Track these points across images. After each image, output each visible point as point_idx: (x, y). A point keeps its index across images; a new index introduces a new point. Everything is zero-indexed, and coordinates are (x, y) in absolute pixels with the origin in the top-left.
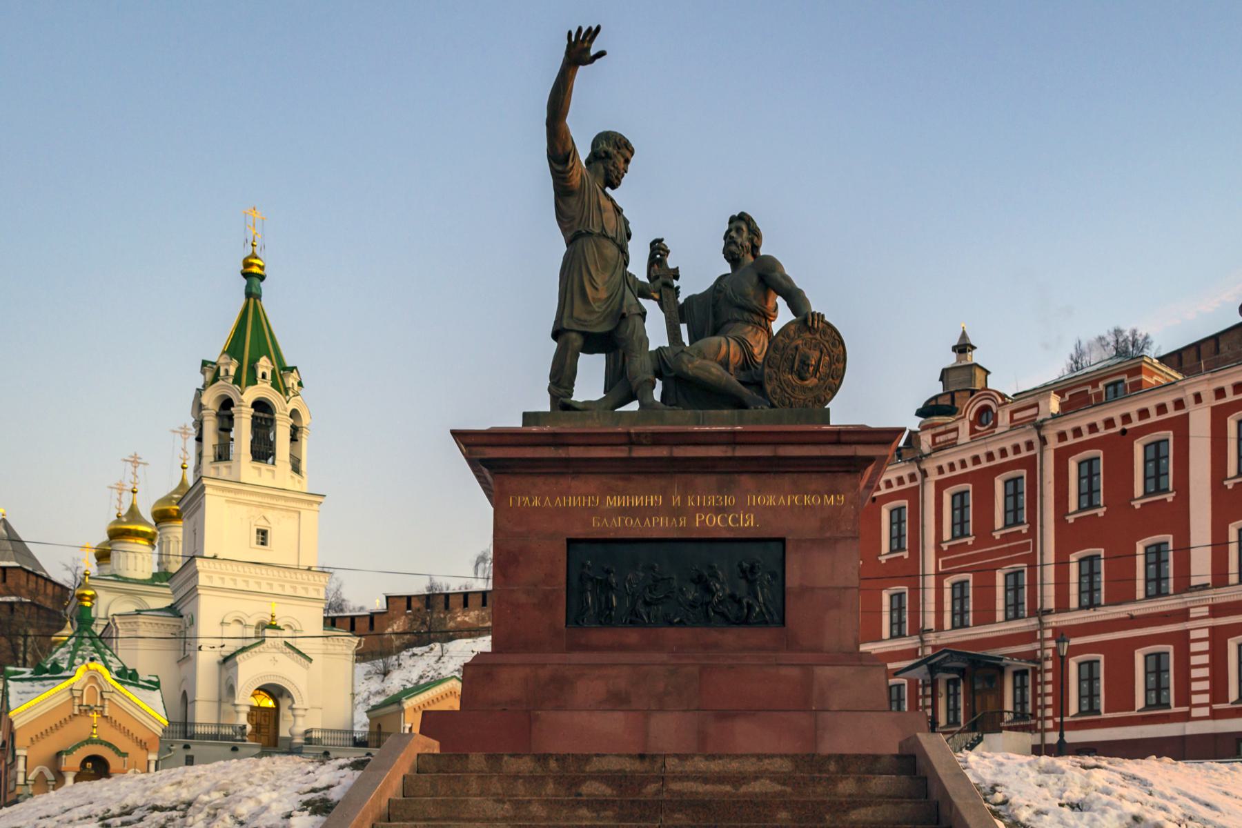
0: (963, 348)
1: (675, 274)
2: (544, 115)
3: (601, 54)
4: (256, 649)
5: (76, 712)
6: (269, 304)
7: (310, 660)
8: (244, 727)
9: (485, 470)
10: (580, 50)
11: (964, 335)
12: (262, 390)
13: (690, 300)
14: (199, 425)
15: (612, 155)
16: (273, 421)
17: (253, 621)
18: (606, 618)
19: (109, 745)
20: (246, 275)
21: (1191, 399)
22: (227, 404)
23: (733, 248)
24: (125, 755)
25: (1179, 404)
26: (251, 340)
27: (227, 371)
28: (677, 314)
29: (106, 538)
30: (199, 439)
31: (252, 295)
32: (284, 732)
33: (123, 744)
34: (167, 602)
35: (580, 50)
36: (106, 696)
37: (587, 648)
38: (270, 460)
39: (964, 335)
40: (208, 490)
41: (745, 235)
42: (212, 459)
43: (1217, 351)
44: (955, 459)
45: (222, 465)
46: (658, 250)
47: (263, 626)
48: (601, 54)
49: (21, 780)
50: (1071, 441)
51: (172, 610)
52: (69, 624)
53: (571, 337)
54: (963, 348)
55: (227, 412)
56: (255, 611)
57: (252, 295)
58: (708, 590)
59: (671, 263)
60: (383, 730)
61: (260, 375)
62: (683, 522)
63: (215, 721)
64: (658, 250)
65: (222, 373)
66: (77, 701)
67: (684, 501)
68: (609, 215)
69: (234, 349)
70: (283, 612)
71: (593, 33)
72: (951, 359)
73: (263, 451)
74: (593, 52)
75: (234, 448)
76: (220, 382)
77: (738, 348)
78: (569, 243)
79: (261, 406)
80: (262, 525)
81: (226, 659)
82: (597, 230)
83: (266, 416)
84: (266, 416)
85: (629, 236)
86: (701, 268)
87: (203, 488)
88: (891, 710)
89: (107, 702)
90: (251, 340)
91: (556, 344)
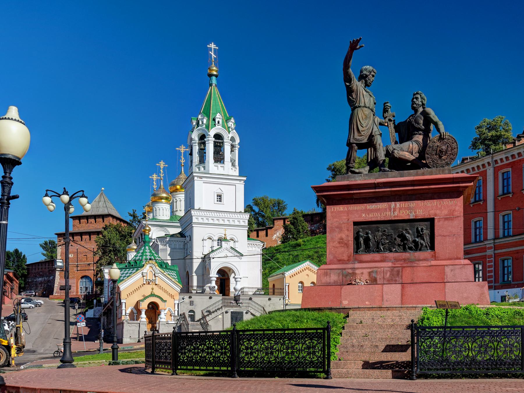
4: (219, 251)
5: (145, 283)
8: (214, 287)
10: (353, 46)
13: (398, 124)
16: (223, 143)
17: (216, 238)
18: (368, 249)
22: (202, 138)
23: (415, 105)
24: (165, 301)
32: (43, 258)
33: (165, 296)
34: (179, 230)
35: (353, 46)
36: (156, 275)
37: (361, 262)
38: (222, 161)
40: (196, 178)
41: (420, 100)
47: (220, 240)
49: (124, 313)
51: (181, 234)
55: (203, 141)
56: (217, 233)
61: (217, 122)
65: (200, 123)
70: (230, 233)
71: (358, 41)
73: (219, 157)
77: (417, 145)
79: (218, 136)
82: (362, 105)
83: (220, 141)
84: (220, 141)
87: (193, 177)
88: (475, 281)
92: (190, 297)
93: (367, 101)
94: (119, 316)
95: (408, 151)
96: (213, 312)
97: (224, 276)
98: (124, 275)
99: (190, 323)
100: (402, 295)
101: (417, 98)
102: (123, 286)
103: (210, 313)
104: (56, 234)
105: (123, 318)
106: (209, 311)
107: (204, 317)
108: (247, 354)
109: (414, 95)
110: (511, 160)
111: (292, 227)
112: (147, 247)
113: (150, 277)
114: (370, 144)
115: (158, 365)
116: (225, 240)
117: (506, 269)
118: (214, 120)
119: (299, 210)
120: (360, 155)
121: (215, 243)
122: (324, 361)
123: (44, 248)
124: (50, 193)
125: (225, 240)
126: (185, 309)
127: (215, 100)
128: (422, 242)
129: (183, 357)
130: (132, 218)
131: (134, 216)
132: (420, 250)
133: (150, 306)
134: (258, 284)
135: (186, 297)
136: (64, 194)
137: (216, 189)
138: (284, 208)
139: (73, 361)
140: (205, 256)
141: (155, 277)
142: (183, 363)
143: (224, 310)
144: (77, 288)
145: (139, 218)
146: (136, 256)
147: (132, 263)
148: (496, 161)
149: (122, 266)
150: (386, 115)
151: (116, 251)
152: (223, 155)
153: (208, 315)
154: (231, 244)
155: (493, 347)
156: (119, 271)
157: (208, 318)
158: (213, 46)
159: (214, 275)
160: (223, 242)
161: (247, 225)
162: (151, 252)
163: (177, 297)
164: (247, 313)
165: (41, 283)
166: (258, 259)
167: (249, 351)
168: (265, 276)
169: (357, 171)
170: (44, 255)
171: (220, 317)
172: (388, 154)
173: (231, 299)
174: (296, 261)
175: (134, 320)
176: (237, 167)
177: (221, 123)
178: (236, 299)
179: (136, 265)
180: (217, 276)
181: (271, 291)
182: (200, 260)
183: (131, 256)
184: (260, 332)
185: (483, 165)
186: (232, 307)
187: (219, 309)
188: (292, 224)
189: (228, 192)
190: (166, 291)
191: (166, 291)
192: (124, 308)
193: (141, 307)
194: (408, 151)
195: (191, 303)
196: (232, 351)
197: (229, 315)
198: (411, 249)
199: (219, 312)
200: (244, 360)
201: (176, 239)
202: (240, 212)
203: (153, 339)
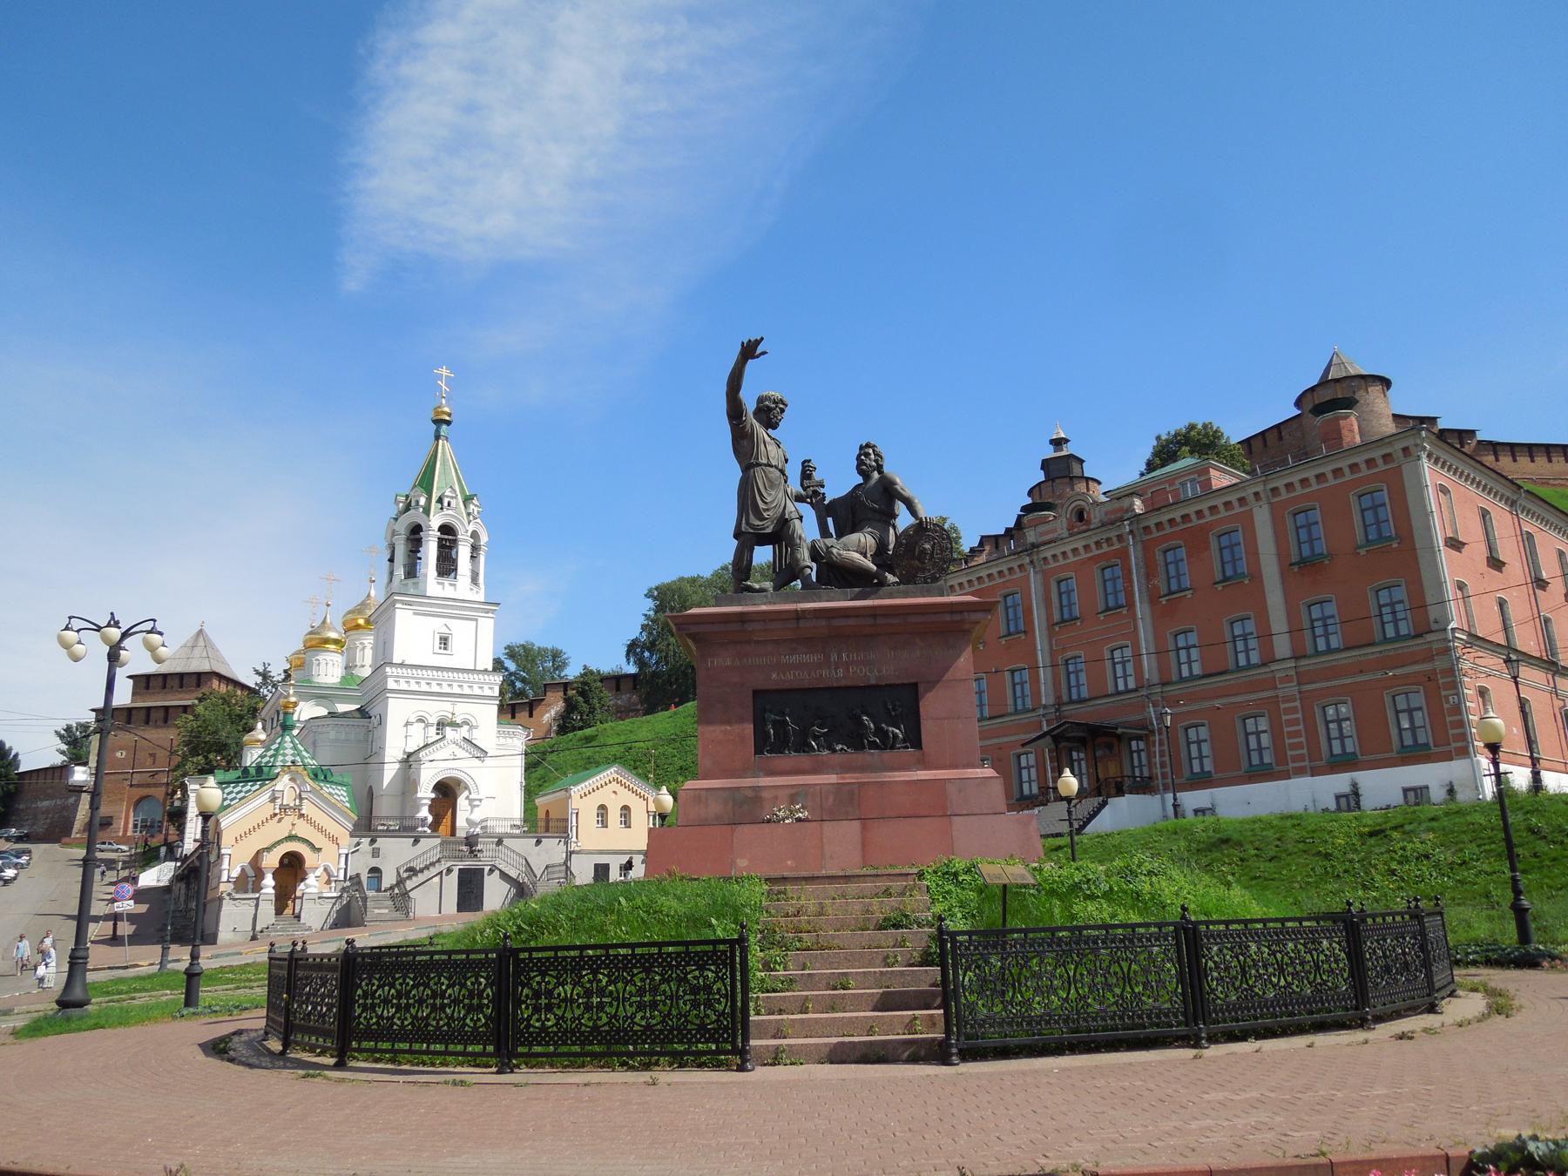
2: (724, 389)
3: (764, 353)
9: (690, 642)
10: (749, 351)
15: (769, 413)
16: (455, 542)
17: (434, 720)
18: (780, 747)
21: (1252, 497)
24: (319, 850)
25: (1120, 538)
28: (825, 511)
29: (301, 647)
30: (391, 560)
33: (318, 840)
35: (749, 351)
43: (1281, 438)
44: (1058, 551)
45: (410, 581)
47: (441, 725)
48: (764, 353)
49: (225, 878)
50: (1284, 495)
51: (363, 713)
53: (747, 539)
56: (436, 710)
59: (817, 476)
62: (841, 672)
63: (396, 814)
67: (840, 657)
70: (461, 710)
71: (758, 342)
72: (1050, 453)
73: (447, 566)
75: (421, 570)
79: (446, 529)
91: (736, 542)
92: (373, 841)
93: (771, 455)
94: (213, 883)
95: (857, 548)
96: (421, 871)
97: (447, 792)
99: (370, 894)
100: (864, 845)
101: (867, 455)
102: (225, 822)
103: (413, 871)
105: (222, 887)
107: (400, 882)
108: (537, 1009)
109: (861, 448)
111: (580, 699)
112: (288, 739)
113: (289, 799)
114: (781, 535)
115: (299, 1036)
116: (453, 724)
118: (440, 500)
119: (593, 668)
120: (763, 555)
121: (433, 730)
122: (734, 1022)
123: (61, 737)
124: (76, 624)
125: (453, 724)
126: (361, 865)
127: (444, 462)
129: (363, 1017)
130: (259, 679)
131: (265, 675)
132: (892, 748)
134: (516, 810)
135: (366, 841)
136: (109, 625)
137: (438, 625)
138: (564, 664)
139: (87, 1002)
140: (409, 755)
141: (301, 799)
142: (369, 1034)
143: (443, 866)
144: (126, 823)
145: (209, 959)
146: (262, 756)
147: (252, 771)
148: (1275, 490)
149: (232, 775)
150: (806, 483)
151: (221, 748)
152: (454, 562)
153: (409, 878)
154: (464, 731)
156: (219, 792)
157: (409, 885)
158: (444, 372)
159: (426, 793)
160: (448, 729)
162: (295, 748)
163: (347, 842)
164: (491, 871)
165: (47, 811)
166: (519, 762)
168: (529, 793)
169: (757, 586)
170: (63, 753)
171: (437, 879)
172: (815, 554)
173: (460, 843)
174: (591, 765)
175: (246, 892)
176: (482, 586)
178: (471, 841)
179: (261, 775)
181: (542, 824)
182: (397, 766)
183: (251, 757)
184: (572, 953)
186: (461, 859)
187: (433, 864)
188: (582, 693)
189: (461, 631)
190: (321, 830)
191: (321, 830)
192: (225, 865)
193: (265, 864)
194: (857, 548)
196: (499, 1001)
197: (455, 874)
198: (873, 745)
199: (433, 871)
200: (529, 1026)
201: (351, 722)
203: (290, 966)
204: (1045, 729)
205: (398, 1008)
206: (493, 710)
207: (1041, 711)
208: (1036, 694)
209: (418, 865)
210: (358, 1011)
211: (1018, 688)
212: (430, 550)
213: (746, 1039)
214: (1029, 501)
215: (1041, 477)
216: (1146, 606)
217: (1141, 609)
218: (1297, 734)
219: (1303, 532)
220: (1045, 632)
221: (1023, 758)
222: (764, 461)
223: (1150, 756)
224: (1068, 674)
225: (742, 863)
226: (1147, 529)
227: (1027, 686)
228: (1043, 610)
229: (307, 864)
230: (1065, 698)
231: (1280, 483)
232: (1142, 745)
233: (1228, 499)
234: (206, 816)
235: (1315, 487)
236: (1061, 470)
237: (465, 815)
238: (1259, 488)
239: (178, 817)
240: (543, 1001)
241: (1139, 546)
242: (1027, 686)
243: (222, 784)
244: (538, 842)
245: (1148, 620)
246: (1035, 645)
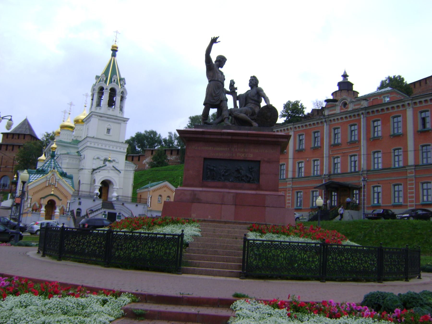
0: (345, 76)
1: (236, 89)
5: (47, 185)
6: (117, 58)
7: (120, 172)
10: (214, 41)
11: (345, 72)
12: (114, 85)
13: (239, 95)
14: (93, 95)
15: (221, 61)
19: (56, 196)
20: (112, 50)
21: (407, 104)
24: (61, 200)
26: (112, 70)
27: (103, 79)
28: (236, 98)
30: (92, 100)
31: (114, 55)
33: (61, 197)
35: (214, 41)
36: (57, 180)
38: (113, 107)
39: (345, 72)
42: (95, 106)
43: (426, 83)
45: (98, 108)
46: (232, 84)
52: (44, 154)
53: (208, 105)
54: (345, 76)
56: (103, 155)
57: (114, 55)
58: (239, 173)
59: (235, 86)
60: (142, 197)
63: (88, 190)
64: (232, 84)
65: (102, 80)
66: (48, 181)
68: (220, 75)
69: (106, 73)
71: (217, 38)
72: (341, 79)
73: (111, 103)
74: (217, 41)
76: (101, 82)
78: (209, 82)
80: (109, 127)
81: (94, 170)
85: (225, 80)
86: (243, 88)
89: (57, 183)
90: (112, 70)
96: (95, 211)
98: (35, 178)
104: (2, 133)
106: (92, 210)
110: (305, 128)
117: (299, 198)
121: (102, 162)
125: (109, 161)
128: (251, 176)
133: (50, 202)
134: (129, 192)
137: (107, 125)
148: (415, 103)
152: (114, 102)
154: (113, 164)
155: (300, 257)
159: (98, 184)
161: (126, 151)
167: (135, 249)
177: (116, 81)
180: (101, 185)
183: (39, 165)
185: (287, 129)
195: (80, 203)
202: (123, 142)
204: (324, 183)
205: (77, 245)
206: (124, 157)
207: (323, 177)
208: (322, 170)
209: (94, 209)
210: (65, 245)
211: (316, 167)
212: (106, 97)
213: (180, 265)
214: (331, 98)
215: (337, 89)
216: (365, 142)
217: (363, 142)
218: (412, 193)
219: (396, 124)
220: (327, 148)
221: (315, 193)
222: (216, 79)
223: (360, 196)
224: (314, 166)
225: (194, 215)
226: (368, 113)
227: (319, 167)
228: (328, 138)
229: (57, 204)
230: (332, 172)
231: (297, 126)
232: (357, 192)
233: (350, 115)
234: (24, 183)
235: (381, 113)
236: (345, 86)
237: (114, 194)
238: (410, 102)
239: (16, 183)
240: (120, 247)
241: (365, 118)
242: (319, 167)
243: (29, 173)
244: (137, 205)
245: (365, 146)
246: (323, 152)
